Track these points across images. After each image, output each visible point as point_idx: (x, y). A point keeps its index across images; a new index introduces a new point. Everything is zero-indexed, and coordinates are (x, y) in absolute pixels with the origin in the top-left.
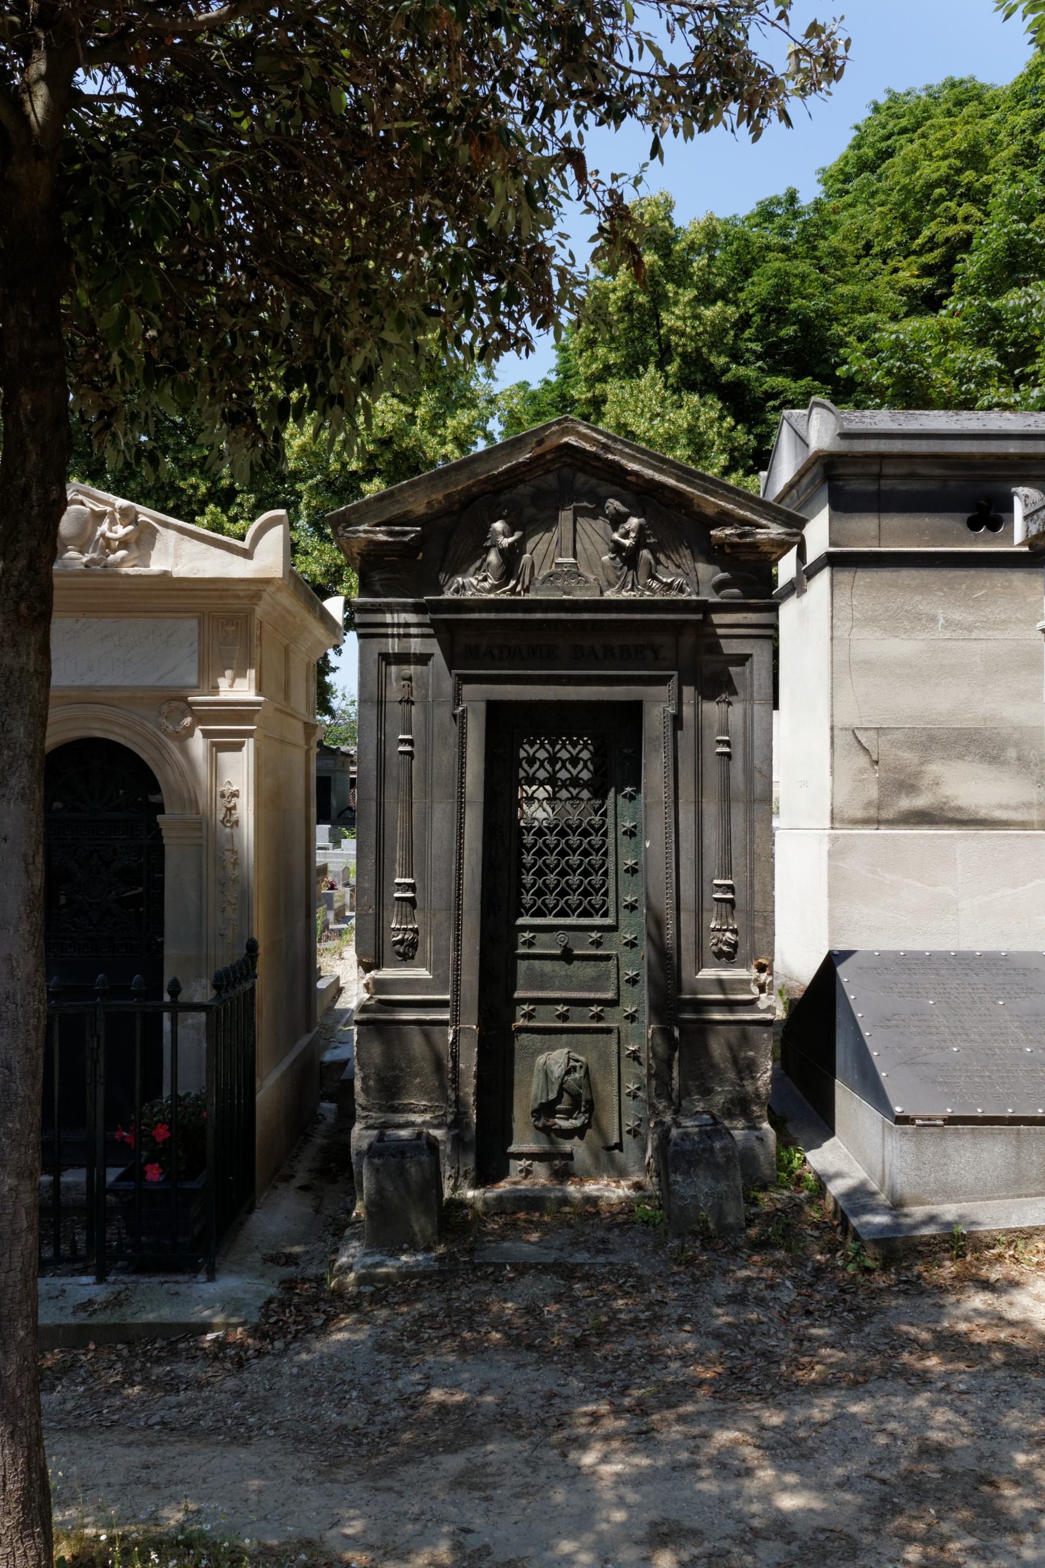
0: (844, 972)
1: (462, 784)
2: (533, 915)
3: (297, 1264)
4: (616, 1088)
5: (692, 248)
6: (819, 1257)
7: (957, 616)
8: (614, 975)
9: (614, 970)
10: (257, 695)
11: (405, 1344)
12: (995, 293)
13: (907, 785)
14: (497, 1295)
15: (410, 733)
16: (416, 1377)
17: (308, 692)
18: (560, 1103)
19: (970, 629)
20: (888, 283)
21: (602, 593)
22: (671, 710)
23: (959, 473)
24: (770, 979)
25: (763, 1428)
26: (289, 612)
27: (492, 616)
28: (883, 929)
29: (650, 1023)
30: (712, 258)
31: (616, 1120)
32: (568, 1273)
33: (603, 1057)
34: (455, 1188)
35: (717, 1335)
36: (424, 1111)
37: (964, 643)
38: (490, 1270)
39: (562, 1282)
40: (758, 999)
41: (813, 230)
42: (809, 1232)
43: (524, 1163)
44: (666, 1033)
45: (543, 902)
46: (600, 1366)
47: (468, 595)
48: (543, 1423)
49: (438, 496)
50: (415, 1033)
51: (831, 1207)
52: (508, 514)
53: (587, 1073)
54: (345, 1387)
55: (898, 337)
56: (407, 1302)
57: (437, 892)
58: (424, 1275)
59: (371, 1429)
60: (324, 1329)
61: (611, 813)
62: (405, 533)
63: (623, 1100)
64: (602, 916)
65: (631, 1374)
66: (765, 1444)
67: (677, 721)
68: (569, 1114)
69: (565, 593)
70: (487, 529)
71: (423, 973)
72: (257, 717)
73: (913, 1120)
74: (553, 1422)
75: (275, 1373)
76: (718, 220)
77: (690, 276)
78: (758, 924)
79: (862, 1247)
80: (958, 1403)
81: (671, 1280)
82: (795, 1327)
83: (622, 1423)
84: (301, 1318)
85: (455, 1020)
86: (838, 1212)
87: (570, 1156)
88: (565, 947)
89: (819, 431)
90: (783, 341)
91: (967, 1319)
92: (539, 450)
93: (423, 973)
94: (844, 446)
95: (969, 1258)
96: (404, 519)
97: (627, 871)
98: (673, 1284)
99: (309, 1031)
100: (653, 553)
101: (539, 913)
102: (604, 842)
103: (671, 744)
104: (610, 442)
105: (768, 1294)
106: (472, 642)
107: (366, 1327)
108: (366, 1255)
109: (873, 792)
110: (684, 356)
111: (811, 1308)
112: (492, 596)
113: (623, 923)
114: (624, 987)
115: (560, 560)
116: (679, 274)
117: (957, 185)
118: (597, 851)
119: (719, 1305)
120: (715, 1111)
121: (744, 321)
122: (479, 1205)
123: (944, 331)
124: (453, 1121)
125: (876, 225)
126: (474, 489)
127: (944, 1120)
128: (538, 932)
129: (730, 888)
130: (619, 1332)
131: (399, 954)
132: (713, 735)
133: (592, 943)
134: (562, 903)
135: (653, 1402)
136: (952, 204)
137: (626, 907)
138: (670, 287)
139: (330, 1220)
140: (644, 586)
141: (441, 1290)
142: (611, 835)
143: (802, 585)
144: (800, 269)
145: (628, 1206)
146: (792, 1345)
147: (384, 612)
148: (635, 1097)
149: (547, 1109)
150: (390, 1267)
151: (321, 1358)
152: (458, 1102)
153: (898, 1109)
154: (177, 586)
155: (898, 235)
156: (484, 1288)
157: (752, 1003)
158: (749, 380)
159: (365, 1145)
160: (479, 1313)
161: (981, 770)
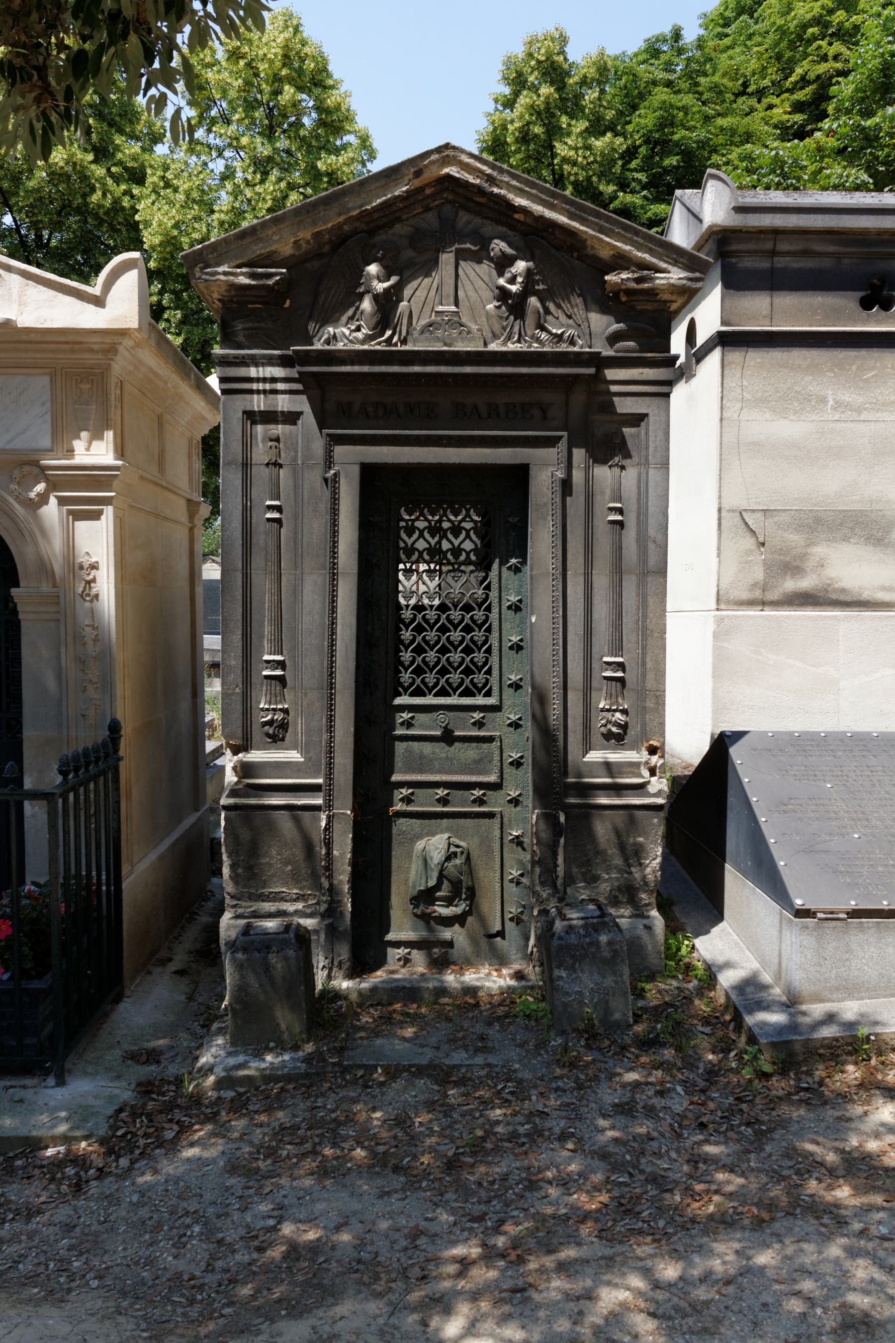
0: (736, 753)
1: (334, 554)
2: (412, 695)
3: (158, 1062)
4: (498, 875)
5: (584, 82)
6: (710, 1057)
7: (846, 397)
8: (497, 758)
9: (497, 752)
10: (117, 459)
11: (261, 1164)
12: (868, 114)
13: (791, 566)
14: (365, 1103)
15: (278, 499)
16: (264, 1207)
17: (190, 468)
18: (440, 890)
19: (859, 411)
20: (763, 119)
21: (486, 345)
22: (560, 475)
23: (854, 250)
24: (661, 761)
25: (657, 1285)
26: (157, 375)
27: (366, 369)
28: (769, 708)
29: (534, 809)
30: (603, 91)
31: (499, 907)
32: (443, 1076)
33: (485, 842)
34: (329, 977)
35: (603, 1155)
36: (296, 900)
37: (850, 425)
38: (360, 1073)
39: (436, 1087)
40: (648, 783)
41: (695, 66)
42: (701, 1029)
43: (402, 951)
44: (549, 818)
45: (423, 681)
46: (474, 1193)
47: (340, 346)
48: (404, 1273)
49: (306, 234)
50: (284, 821)
51: (722, 1000)
52: (384, 256)
53: (468, 858)
54: (188, 1221)
55: (777, 154)
56: (269, 1110)
57: (308, 670)
58: (288, 1078)
59: (211, 1279)
60: (172, 1147)
61: (495, 586)
62: (270, 276)
63: (503, 889)
64: (485, 696)
65: (507, 1204)
66: (660, 1311)
67: (566, 486)
68: (449, 902)
69: (445, 344)
70: (360, 273)
71: (294, 756)
72: (116, 483)
73: (815, 913)
74: (416, 1272)
75: (113, 1199)
76: (608, 56)
77: (582, 109)
78: (650, 704)
79: (760, 1051)
80: (881, 1253)
81: (554, 1085)
82: (688, 1143)
83: (492, 1274)
84: (152, 1130)
85: (329, 805)
86: (729, 1004)
87: (450, 944)
88: (445, 728)
89: (713, 204)
90: (666, 171)
91: (877, 1136)
92: (417, 183)
93: (294, 756)
94: (738, 221)
95: (873, 1062)
96: (268, 260)
97: (511, 648)
98: (557, 1090)
99: (197, 810)
100: (542, 301)
101: (418, 693)
102: (487, 617)
103: (559, 512)
104: (495, 174)
105: (658, 1102)
106: (344, 398)
107: (221, 1141)
108: (229, 1054)
109: (758, 574)
110: (576, 184)
111: (704, 1119)
112: (366, 347)
113: (507, 703)
114: (507, 770)
115: (440, 308)
116: (574, 108)
117: (827, 25)
118: (480, 627)
119: (604, 1116)
120: (602, 899)
121: (630, 153)
122: (354, 997)
123: (820, 149)
124: (326, 910)
125: (754, 64)
126: (346, 228)
127: (848, 913)
128: (417, 714)
129: (621, 666)
130: (496, 1150)
131: (268, 735)
132: (604, 501)
133: (474, 724)
134: (443, 681)
135: (532, 1243)
136: (823, 43)
137: (510, 686)
138: (564, 119)
139: (202, 1008)
140: (532, 337)
141: (307, 1096)
142: (495, 610)
143: (691, 370)
144: (684, 102)
145: (508, 996)
146: (686, 1168)
147: (248, 366)
148: (518, 883)
149: (427, 896)
150: (254, 1068)
151: (166, 1181)
152: (332, 890)
153: (798, 902)
154: (24, 338)
155: (773, 75)
156: (352, 1094)
157: (640, 788)
158: (635, 207)
159: (233, 934)
160: (345, 1123)
161: (866, 552)
